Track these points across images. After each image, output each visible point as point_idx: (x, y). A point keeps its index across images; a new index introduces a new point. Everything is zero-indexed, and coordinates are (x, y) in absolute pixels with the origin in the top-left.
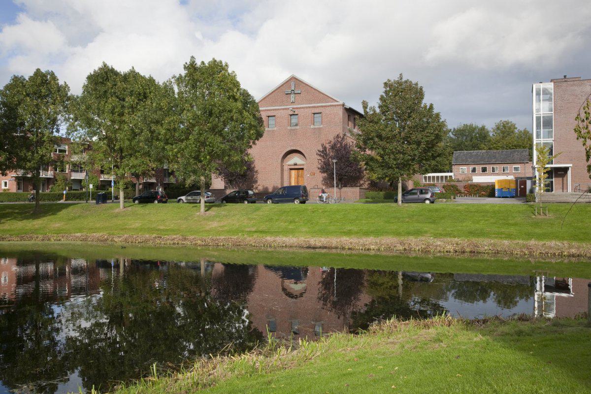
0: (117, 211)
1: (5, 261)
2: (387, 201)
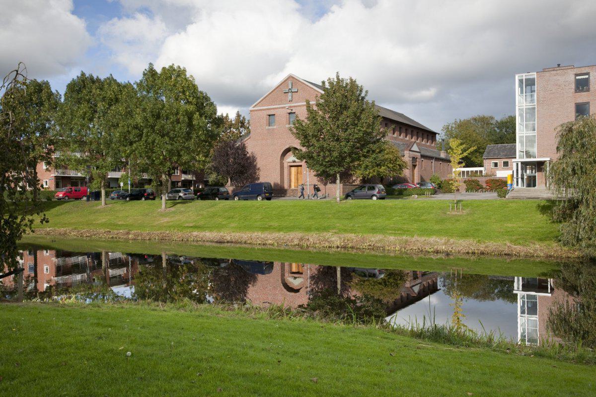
1: (47, 252)
2: (390, 196)
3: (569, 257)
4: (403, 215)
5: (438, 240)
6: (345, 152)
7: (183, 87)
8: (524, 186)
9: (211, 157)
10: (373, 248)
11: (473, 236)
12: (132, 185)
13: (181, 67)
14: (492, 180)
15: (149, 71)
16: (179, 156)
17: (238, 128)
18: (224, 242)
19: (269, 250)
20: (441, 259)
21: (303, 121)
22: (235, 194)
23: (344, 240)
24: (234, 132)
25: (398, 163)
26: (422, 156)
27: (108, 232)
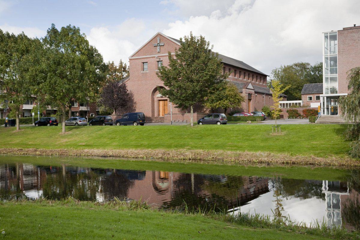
0: (14, 131)
3: (356, 166)
4: (239, 135)
5: (263, 154)
6: (197, 90)
7: (78, 42)
8: (329, 114)
9: (101, 93)
10: (214, 160)
11: (288, 151)
12: (41, 115)
13: (76, 27)
14: (308, 110)
15: (52, 30)
16: (75, 93)
17: (121, 72)
18: (108, 157)
19: (141, 162)
20: (265, 167)
21: (166, 67)
22: (117, 122)
23: (195, 154)
24: (118, 75)
25: (237, 98)
26: (256, 92)
27: (20, 150)
